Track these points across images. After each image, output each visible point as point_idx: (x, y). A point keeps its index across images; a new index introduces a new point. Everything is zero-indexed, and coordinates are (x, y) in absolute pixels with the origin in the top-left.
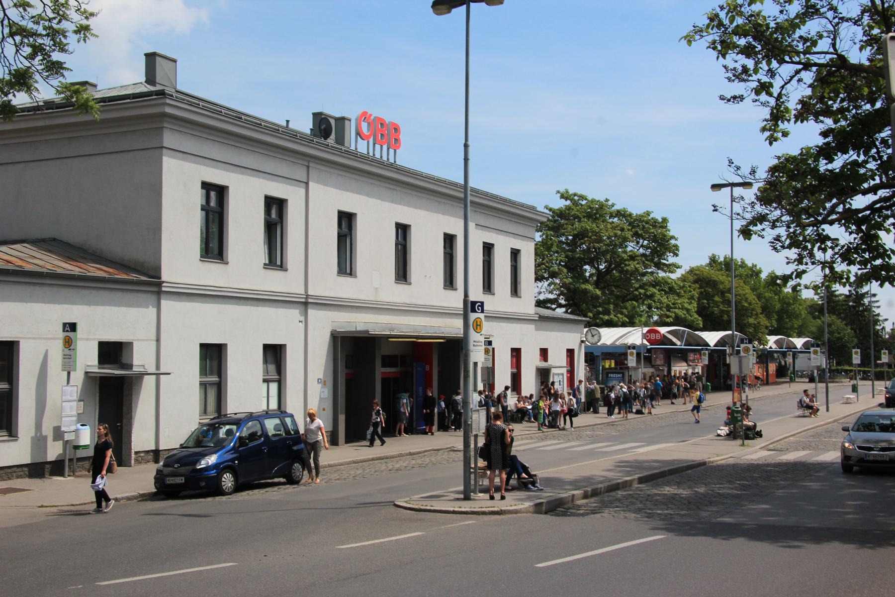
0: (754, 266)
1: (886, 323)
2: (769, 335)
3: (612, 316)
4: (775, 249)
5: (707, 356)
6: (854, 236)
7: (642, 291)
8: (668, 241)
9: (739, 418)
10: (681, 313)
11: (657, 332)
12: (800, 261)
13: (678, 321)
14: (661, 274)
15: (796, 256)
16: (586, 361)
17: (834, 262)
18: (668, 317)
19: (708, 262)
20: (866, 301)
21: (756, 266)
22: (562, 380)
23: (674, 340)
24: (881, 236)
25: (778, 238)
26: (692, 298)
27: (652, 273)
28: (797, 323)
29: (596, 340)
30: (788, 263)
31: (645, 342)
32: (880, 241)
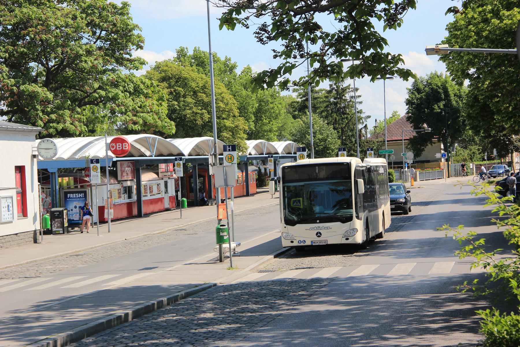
0: (228, 60)
1: (368, 120)
2: (249, 139)
3: (68, 124)
4: (261, 40)
5: (182, 166)
6: (345, 23)
7: (103, 93)
8: (130, 31)
9: (225, 238)
10: (150, 118)
11: (123, 141)
12: (287, 53)
13: (147, 128)
14: (123, 72)
15: (283, 48)
16: (39, 181)
17: (324, 55)
18: (135, 123)
19: (176, 56)
20: (347, 96)
21: (230, 59)
22: (11, 205)
23: (143, 150)
24: (373, 24)
25: (263, 28)
26: (161, 99)
27: (113, 70)
28: (275, 125)
29: (52, 155)
30: (275, 57)
31: (110, 153)
32: (372, 29)
